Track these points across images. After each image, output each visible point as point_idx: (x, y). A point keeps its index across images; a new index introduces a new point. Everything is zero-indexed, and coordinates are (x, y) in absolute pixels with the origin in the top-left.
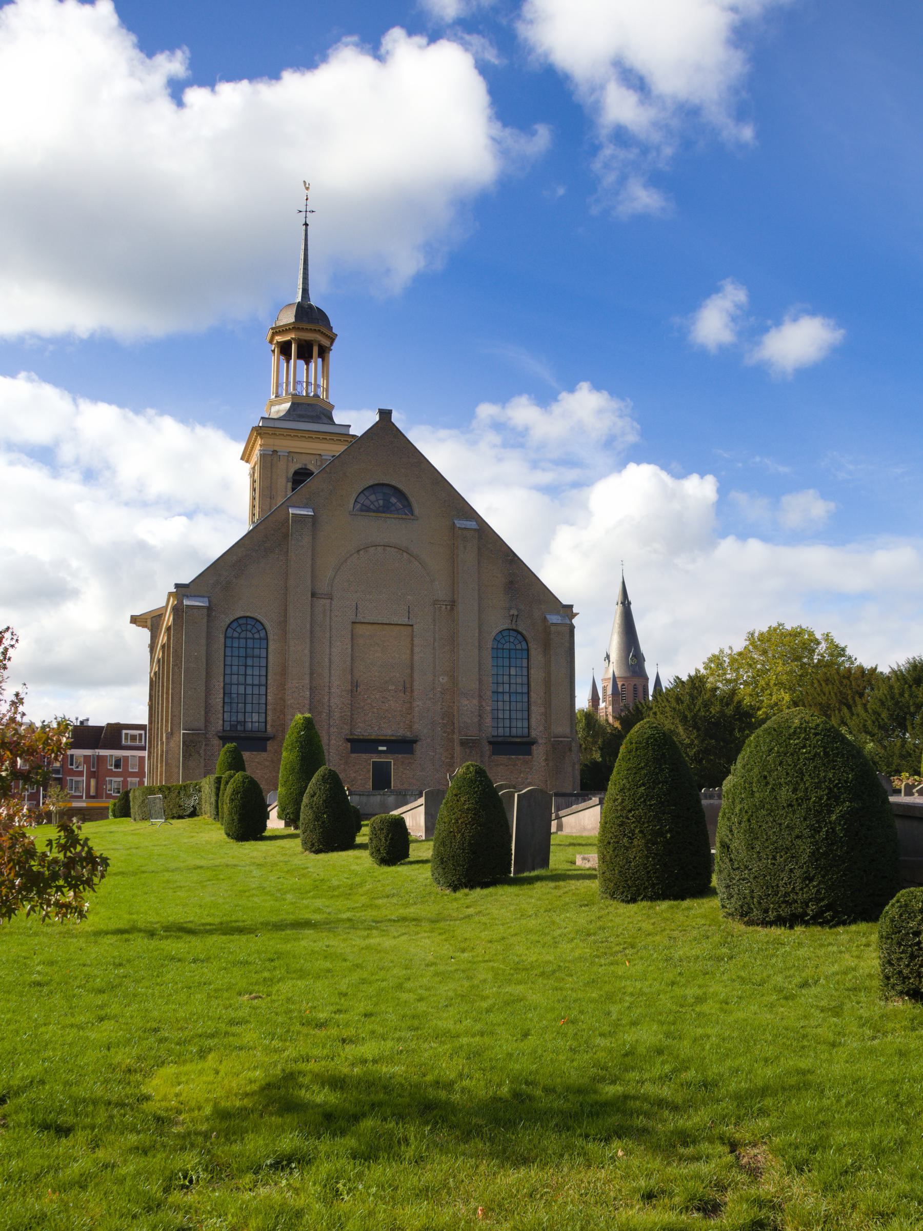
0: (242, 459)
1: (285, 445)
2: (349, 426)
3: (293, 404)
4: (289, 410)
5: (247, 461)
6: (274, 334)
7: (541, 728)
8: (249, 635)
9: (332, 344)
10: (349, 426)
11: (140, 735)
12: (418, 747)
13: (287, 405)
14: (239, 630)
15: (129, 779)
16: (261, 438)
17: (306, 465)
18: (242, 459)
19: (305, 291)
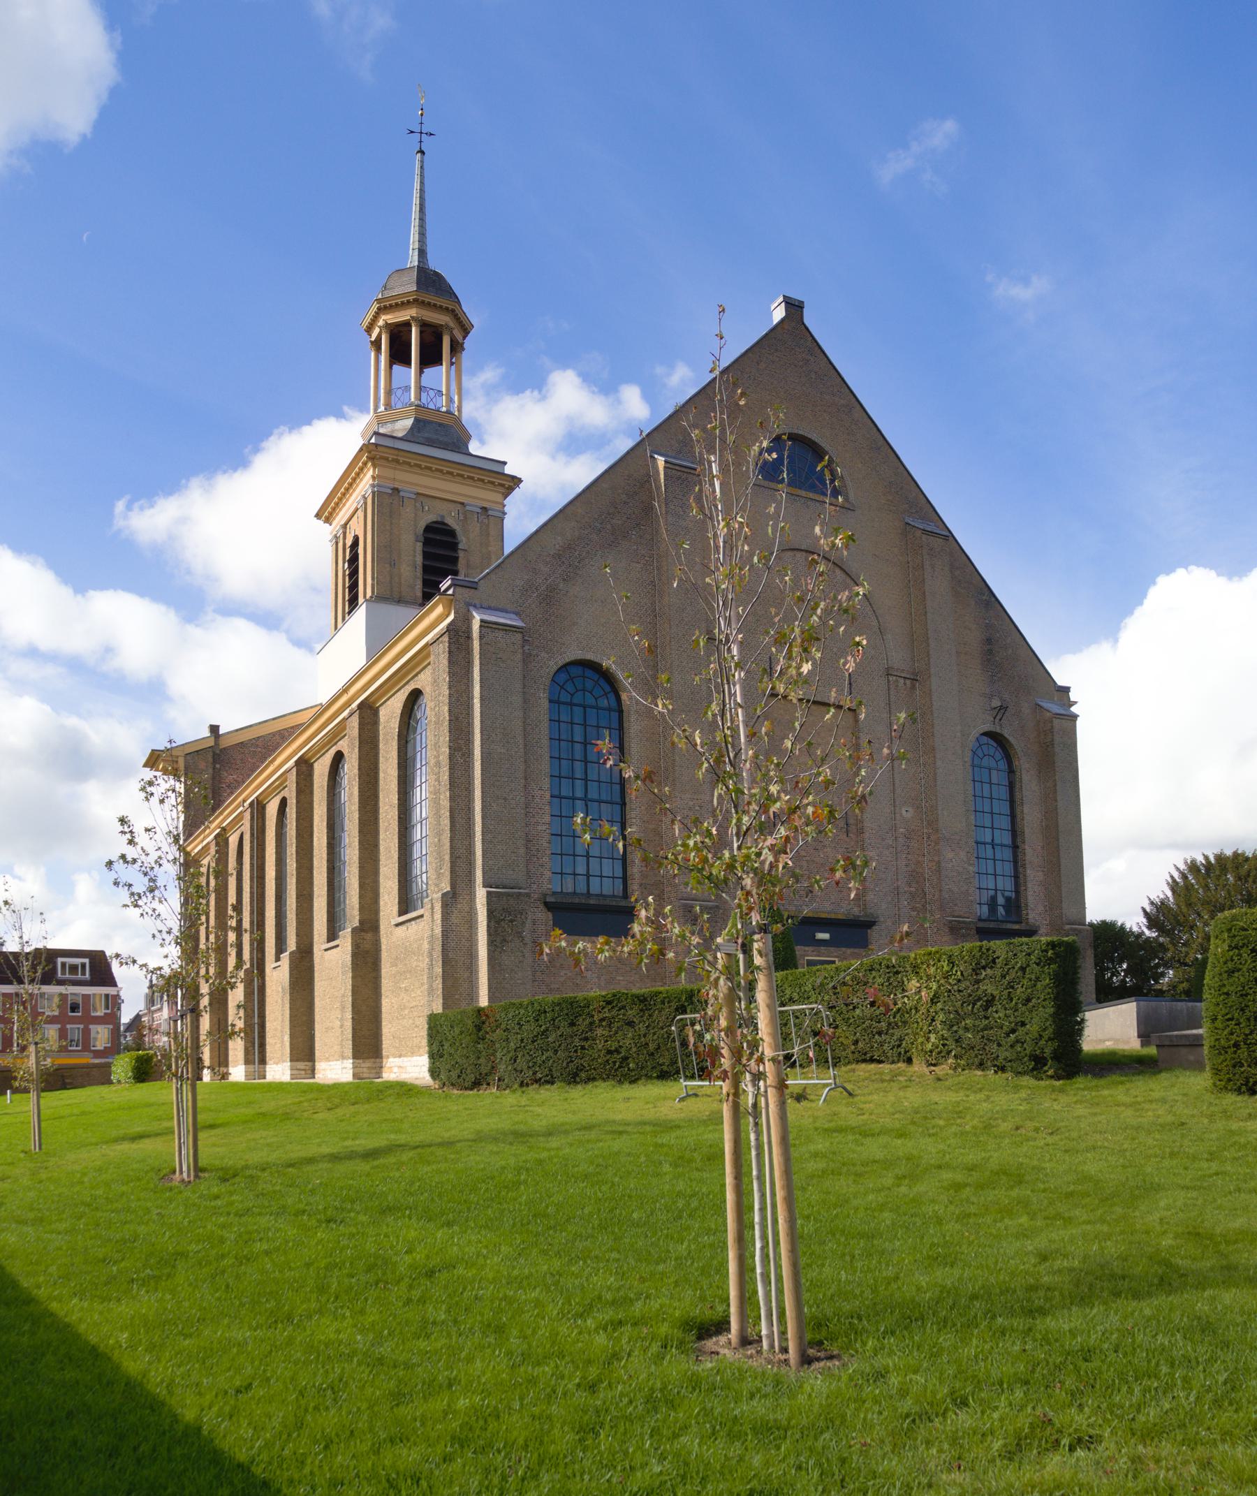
0: (318, 516)
1: (413, 482)
2: (505, 463)
3: (417, 420)
4: (412, 428)
5: (328, 520)
6: (381, 311)
7: (1041, 908)
8: (590, 700)
9: (464, 338)
10: (505, 463)
11: (83, 965)
12: (874, 934)
13: (409, 422)
14: (569, 687)
15: (68, 1026)
16: (374, 466)
17: (443, 517)
18: (318, 516)
19: (422, 253)
